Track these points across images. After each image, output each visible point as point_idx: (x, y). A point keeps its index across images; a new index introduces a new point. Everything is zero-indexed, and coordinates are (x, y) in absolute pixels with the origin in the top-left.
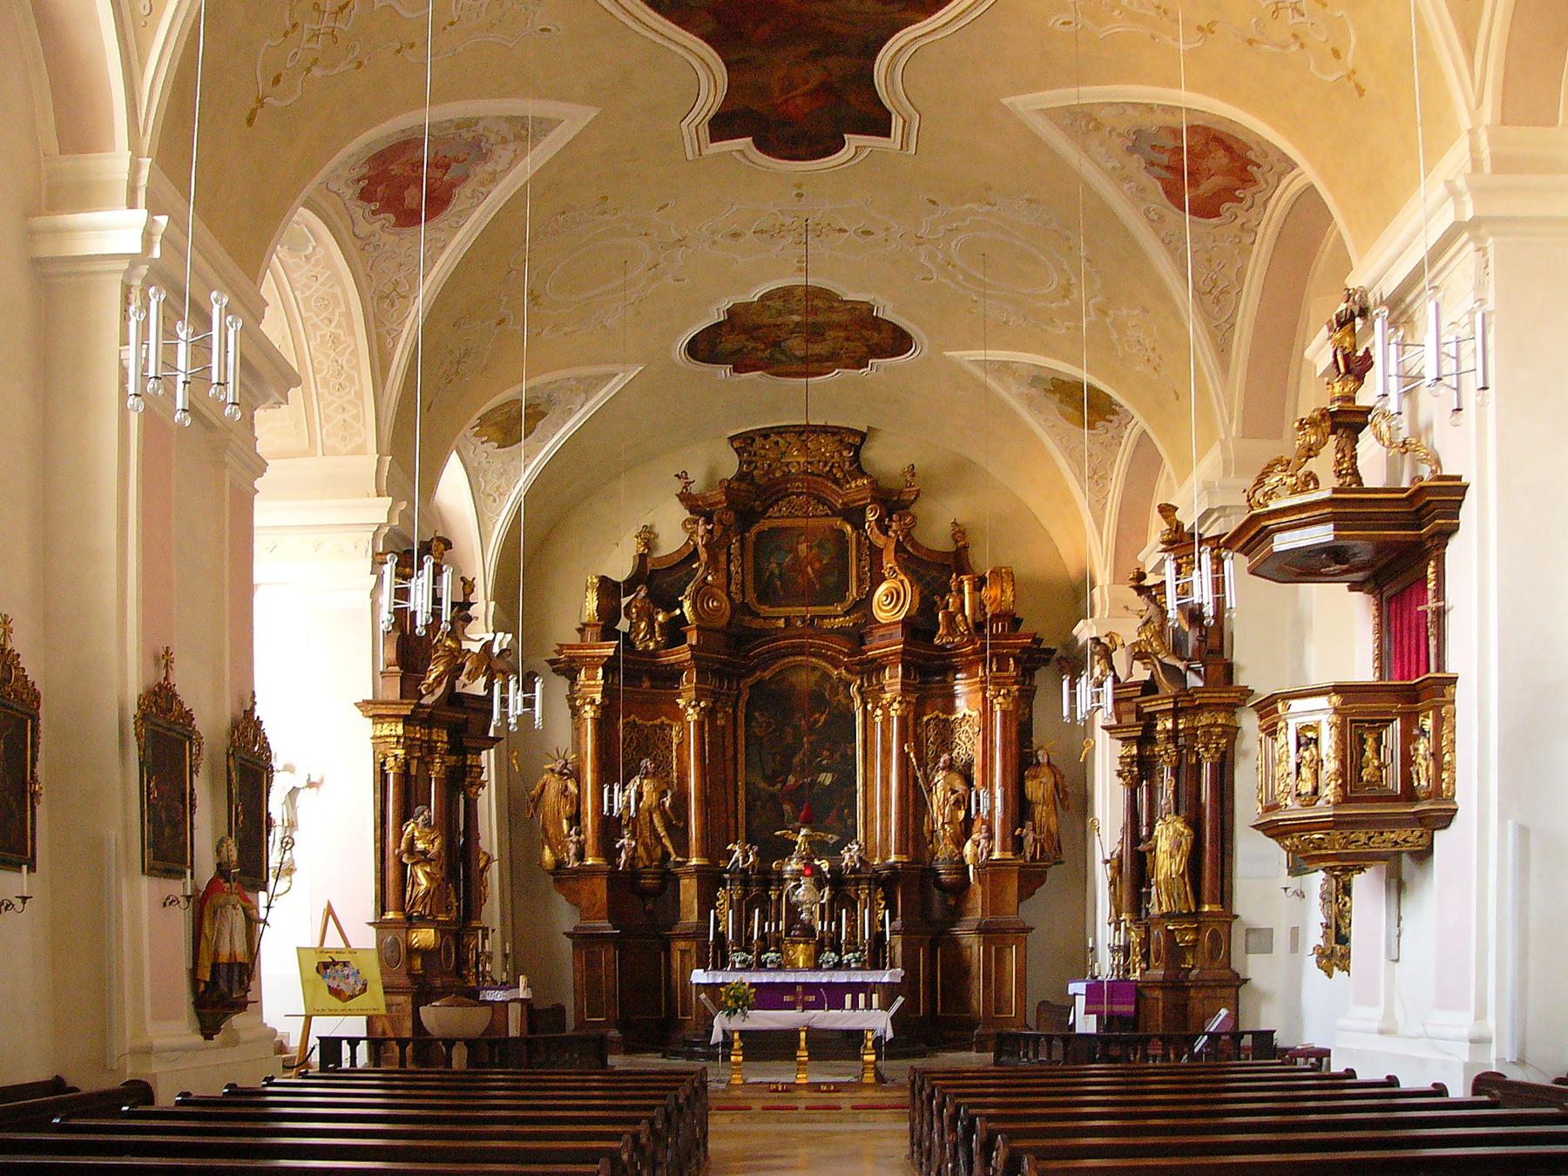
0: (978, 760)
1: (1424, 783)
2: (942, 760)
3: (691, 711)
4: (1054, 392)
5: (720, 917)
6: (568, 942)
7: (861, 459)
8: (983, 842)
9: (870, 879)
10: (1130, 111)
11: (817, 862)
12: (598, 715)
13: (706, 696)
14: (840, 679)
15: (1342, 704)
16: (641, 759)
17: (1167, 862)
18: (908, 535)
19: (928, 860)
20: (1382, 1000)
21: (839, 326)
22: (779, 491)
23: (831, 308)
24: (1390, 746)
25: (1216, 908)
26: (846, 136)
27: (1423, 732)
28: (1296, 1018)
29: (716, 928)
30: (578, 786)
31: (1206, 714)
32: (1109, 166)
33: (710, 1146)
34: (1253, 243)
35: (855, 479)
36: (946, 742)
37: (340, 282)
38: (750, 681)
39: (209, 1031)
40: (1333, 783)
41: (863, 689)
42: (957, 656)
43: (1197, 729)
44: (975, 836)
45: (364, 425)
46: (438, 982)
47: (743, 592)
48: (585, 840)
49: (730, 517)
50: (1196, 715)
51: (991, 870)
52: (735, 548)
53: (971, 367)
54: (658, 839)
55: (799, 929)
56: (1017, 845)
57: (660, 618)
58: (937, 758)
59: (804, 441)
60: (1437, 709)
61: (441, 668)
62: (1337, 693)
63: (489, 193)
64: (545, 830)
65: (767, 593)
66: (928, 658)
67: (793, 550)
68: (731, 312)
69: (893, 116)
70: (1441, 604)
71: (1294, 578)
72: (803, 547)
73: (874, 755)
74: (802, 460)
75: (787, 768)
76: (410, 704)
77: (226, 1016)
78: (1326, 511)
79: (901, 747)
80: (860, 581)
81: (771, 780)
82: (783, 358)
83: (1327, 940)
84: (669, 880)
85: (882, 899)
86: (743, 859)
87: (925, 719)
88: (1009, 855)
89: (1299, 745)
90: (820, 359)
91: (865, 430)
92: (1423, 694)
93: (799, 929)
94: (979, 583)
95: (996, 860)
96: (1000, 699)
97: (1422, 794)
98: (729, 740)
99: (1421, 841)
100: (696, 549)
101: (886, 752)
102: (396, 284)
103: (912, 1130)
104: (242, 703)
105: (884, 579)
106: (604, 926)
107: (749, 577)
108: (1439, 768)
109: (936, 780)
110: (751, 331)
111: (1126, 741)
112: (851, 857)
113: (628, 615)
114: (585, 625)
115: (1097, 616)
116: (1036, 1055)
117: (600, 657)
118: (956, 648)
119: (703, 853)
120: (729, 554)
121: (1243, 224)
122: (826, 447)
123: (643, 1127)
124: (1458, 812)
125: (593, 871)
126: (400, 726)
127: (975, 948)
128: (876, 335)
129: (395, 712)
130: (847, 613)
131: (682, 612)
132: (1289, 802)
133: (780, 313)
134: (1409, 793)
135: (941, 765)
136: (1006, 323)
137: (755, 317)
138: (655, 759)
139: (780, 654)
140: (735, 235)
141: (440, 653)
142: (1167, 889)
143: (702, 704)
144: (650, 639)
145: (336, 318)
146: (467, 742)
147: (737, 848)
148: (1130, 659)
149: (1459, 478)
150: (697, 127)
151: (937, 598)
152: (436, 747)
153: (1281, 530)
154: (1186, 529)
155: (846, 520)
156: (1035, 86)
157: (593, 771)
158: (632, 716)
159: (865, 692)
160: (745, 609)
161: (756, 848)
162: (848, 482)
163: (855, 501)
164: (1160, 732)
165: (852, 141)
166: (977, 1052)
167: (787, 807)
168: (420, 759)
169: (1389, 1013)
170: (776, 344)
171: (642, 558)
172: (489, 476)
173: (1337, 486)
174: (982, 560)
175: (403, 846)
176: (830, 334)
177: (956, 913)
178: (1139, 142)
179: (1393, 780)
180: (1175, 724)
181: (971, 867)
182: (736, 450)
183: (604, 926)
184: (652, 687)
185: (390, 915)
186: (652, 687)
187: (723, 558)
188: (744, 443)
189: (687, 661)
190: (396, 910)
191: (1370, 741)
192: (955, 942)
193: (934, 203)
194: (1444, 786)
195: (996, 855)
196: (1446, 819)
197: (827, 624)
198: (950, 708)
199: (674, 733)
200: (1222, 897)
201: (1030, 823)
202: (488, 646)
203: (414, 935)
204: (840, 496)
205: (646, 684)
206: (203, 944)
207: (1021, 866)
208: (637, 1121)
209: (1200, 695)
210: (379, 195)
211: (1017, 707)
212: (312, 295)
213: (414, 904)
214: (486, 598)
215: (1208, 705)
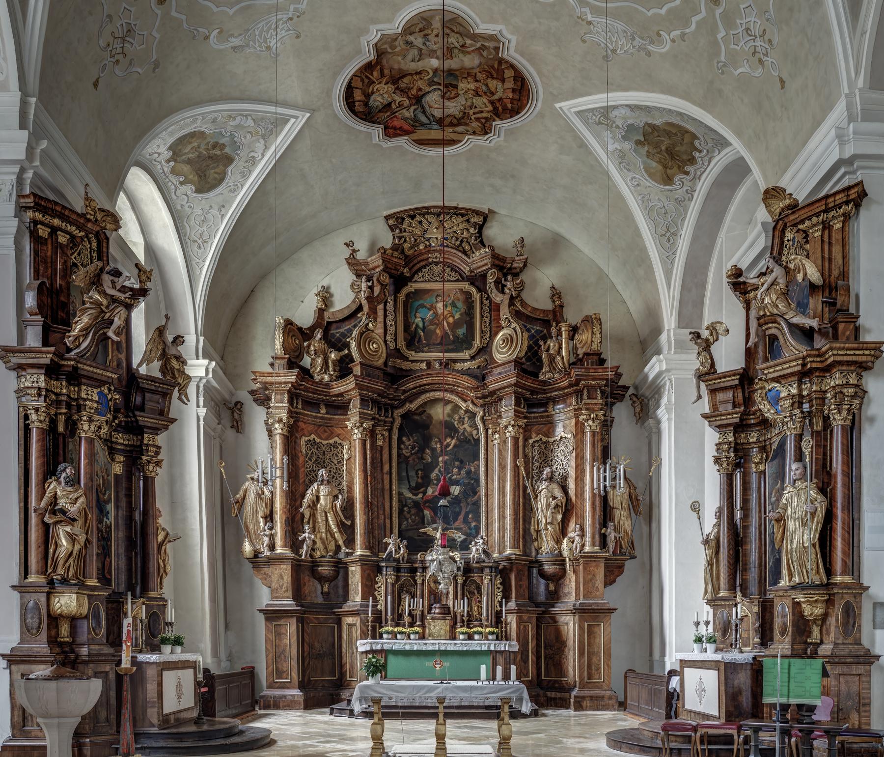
0: (572, 474)
2: (545, 472)
7: (483, 236)
8: (577, 538)
9: (491, 568)
12: (285, 432)
14: (467, 411)
16: (319, 470)
18: (519, 295)
19: (534, 554)
21: (468, 74)
25: (848, 579)
36: (546, 459)
38: (401, 411)
41: (485, 418)
47: (396, 340)
48: (276, 533)
49: (386, 279)
54: (333, 536)
55: (439, 608)
56: (603, 541)
57: (333, 356)
58: (541, 472)
59: (441, 221)
65: (412, 341)
66: (533, 392)
67: (432, 307)
72: (440, 305)
74: (440, 236)
75: (426, 482)
76: (49, 353)
80: (482, 332)
81: (414, 490)
82: (423, 119)
84: (341, 568)
85: (501, 584)
86: (396, 551)
87: (531, 441)
88: (597, 549)
93: (439, 608)
94: (574, 330)
95: (587, 553)
96: (590, 422)
101: (503, 467)
106: (288, 603)
107: (401, 328)
109: (540, 489)
112: (477, 550)
125: (280, 559)
126: (42, 377)
127: (571, 625)
128: (500, 85)
129: (35, 361)
130: (473, 358)
135: (544, 476)
138: (330, 471)
144: (325, 372)
151: (541, 343)
152: (147, 450)
155: (472, 284)
156: (575, 94)
158: (313, 436)
160: (397, 353)
161: (405, 542)
162: (473, 253)
166: (575, 710)
167: (427, 512)
170: (418, 100)
171: (321, 312)
172: (192, 223)
176: (463, 85)
177: (554, 596)
182: (390, 227)
183: (288, 603)
184: (327, 413)
186: (327, 413)
187: (380, 313)
188: (396, 221)
190: (38, 573)
192: (554, 620)
195: (587, 549)
197: (458, 366)
199: (344, 451)
201: (612, 524)
203: (57, 600)
207: (607, 559)
209: (835, 352)
214: (196, 333)
215: (840, 363)
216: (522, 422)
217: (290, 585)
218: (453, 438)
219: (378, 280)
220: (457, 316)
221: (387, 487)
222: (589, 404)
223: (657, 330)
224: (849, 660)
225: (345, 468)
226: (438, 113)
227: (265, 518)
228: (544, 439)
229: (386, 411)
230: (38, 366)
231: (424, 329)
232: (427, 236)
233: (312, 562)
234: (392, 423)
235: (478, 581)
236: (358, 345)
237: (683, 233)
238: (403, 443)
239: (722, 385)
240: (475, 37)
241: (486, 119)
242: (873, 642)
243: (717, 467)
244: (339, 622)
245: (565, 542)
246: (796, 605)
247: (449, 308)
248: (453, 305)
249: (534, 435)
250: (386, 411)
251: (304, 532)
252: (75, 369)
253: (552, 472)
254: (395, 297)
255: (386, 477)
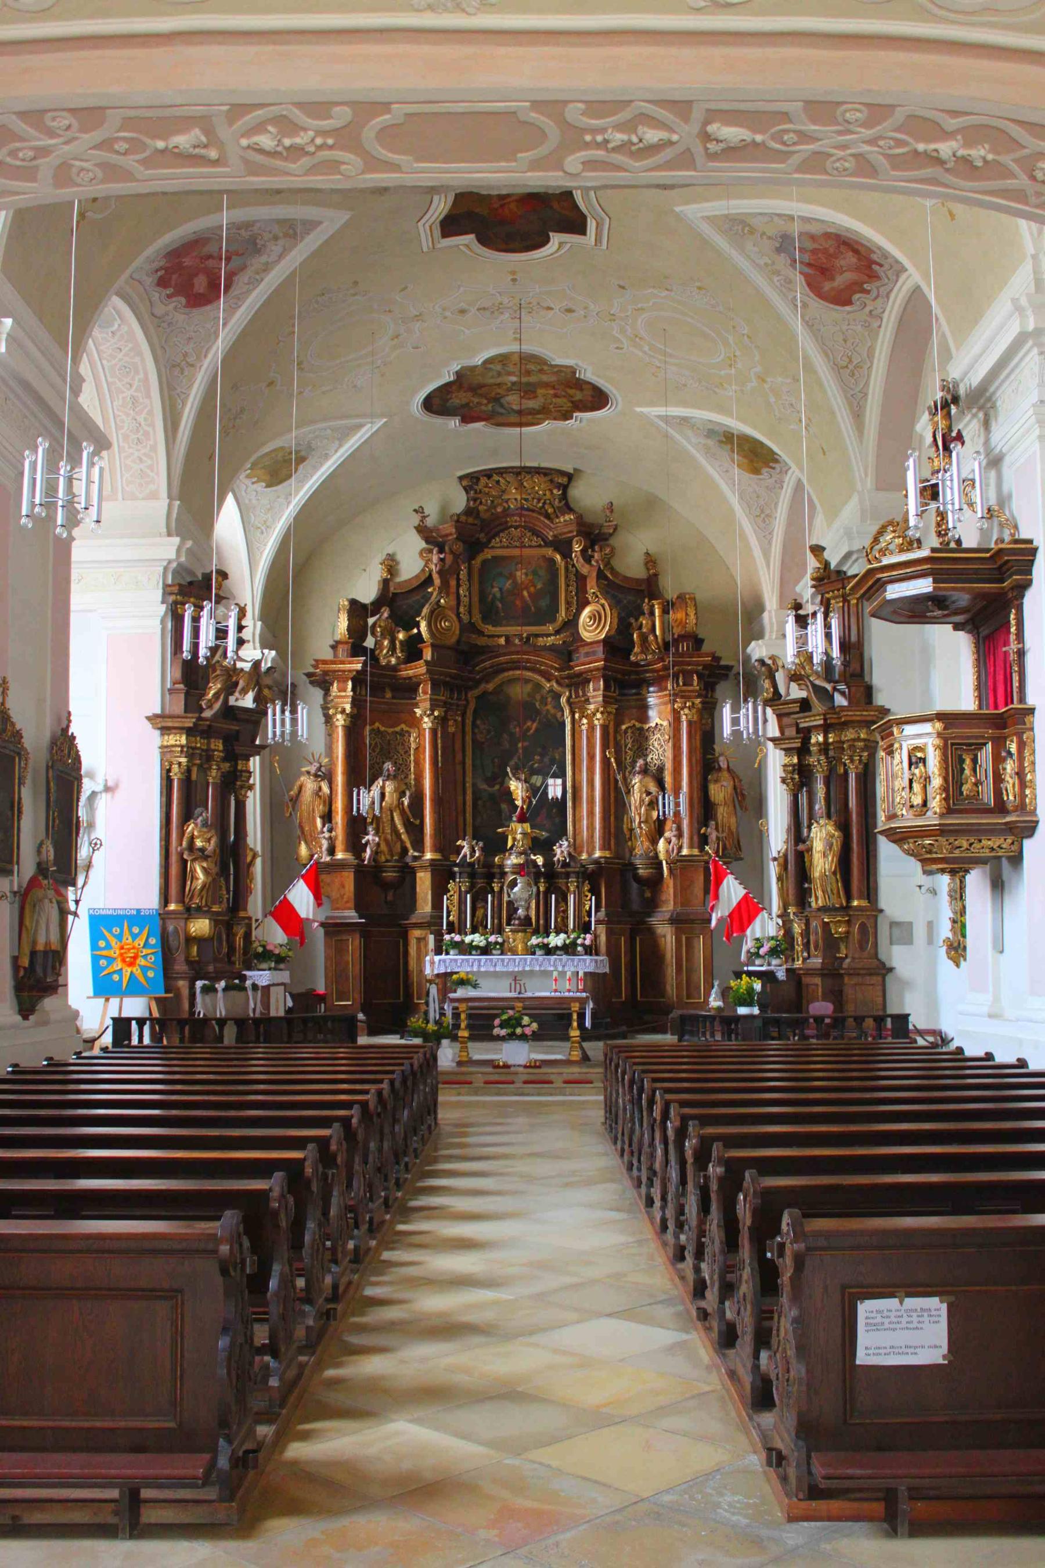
0: (669, 766)
1: (1011, 798)
3: (426, 719)
4: (726, 443)
5: (451, 907)
6: (321, 931)
8: (674, 839)
9: (577, 873)
10: (776, 218)
11: (533, 857)
13: (438, 706)
14: (551, 691)
15: (945, 729)
16: (384, 763)
17: (821, 861)
18: (607, 564)
19: (627, 855)
20: (991, 989)
21: (547, 385)
22: (501, 524)
23: (541, 371)
24: (984, 766)
25: (864, 903)
26: (551, 234)
27: (1010, 754)
28: (933, 1004)
29: (448, 916)
30: (331, 788)
31: (851, 730)
32: (762, 262)
33: (440, 1116)
34: (880, 327)
35: (563, 515)
36: (641, 748)
37: (140, 354)
38: (476, 692)
39: (26, 1010)
40: (938, 797)
42: (647, 671)
43: (844, 743)
44: (667, 834)
45: (157, 474)
46: (211, 968)
48: (336, 837)
49: (459, 547)
50: (842, 730)
51: (680, 865)
52: (463, 574)
53: (656, 420)
54: (398, 835)
57: (401, 636)
58: (634, 762)
60: (1020, 735)
61: (219, 686)
62: (939, 720)
63: (262, 280)
64: (301, 827)
65: (490, 614)
66: (624, 673)
67: (512, 576)
68: (459, 374)
69: (589, 220)
70: (1020, 646)
71: (907, 620)
72: (518, 574)
73: (581, 761)
74: (519, 497)
77: (41, 998)
78: (925, 567)
79: (603, 752)
80: (568, 603)
82: (502, 411)
83: (955, 934)
84: (408, 873)
85: (589, 891)
87: (624, 727)
88: (696, 852)
89: (910, 764)
90: (533, 412)
91: (572, 471)
92: (1009, 721)
96: (686, 711)
97: (1010, 807)
98: (458, 745)
99: (1014, 848)
100: (430, 575)
101: (591, 757)
102: (185, 355)
103: (606, 1101)
104: (59, 720)
105: (588, 603)
106: (351, 915)
107: (476, 599)
108: (1023, 784)
110: (475, 389)
111: (788, 751)
112: (562, 852)
113: (373, 634)
114: (338, 643)
115: (767, 637)
116: (713, 1035)
117: (350, 671)
118: (648, 665)
119: (436, 849)
120: (458, 580)
121: (871, 312)
122: (539, 486)
123: (385, 1086)
124: (1040, 824)
125: (341, 865)
126: (184, 737)
128: (578, 392)
130: (557, 632)
131: (419, 632)
132: (904, 812)
133: (499, 374)
134: (1001, 807)
136: (685, 385)
137: (480, 378)
139: (500, 670)
140: (462, 312)
141: (218, 672)
142: (822, 886)
143: (436, 713)
144: (392, 655)
145: (136, 384)
146: (239, 749)
147: (465, 843)
148: (787, 680)
149: (1030, 542)
150: (431, 227)
151: (632, 620)
153: (892, 581)
154: (832, 567)
155: (557, 549)
157: (343, 773)
158: (377, 724)
159: (574, 703)
161: (481, 844)
162: (557, 517)
163: (565, 533)
164: (814, 745)
165: (556, 238)
168: (200, 766)
169: (996, 999)
170: (497, 400)
171: (386, 583)
173: (938, 546)
174: (670, 588)
175: (185, 844)
176: (540, 391)
177: (652, 905)
178: (784, 244)
179: (988, 796)
180: (826, 737)
181: (664, 863)
183: (351, 915)
184: (393, 697)
185: (172, 907)
186: (393, 697)
187: (453, 583)
188: (471, 482)
189: (423, 675)
191: (968, 761)
192: (651, 931)
193: (623, 288)
194: (1027, 800)
195: (685, 852)
196: (1030, 829)
197: (541, 641)
198: (644, 718)
199: (412, 739)
200: (868, 895)
202: (257, 664)
204: (551, 529)
205: (389, 695)
206: (24, 935)
208: (381, 1081)
210: (173, 283)
211: (701, 718)
212: (116, 365)
213: (192, 897)
214: (254, 618)
215: (852, 722)
216: (612, 709)
217: (352, 895)
218: (534, 721)
219: (450, 549)
220: (539, 586)
221: (459, 778)
222: (684, 691)
223: (760, 608)
224: (862, 972)
225: (412, 758)
226: (516, 407)
227: (322, 817)
228: (638, 725)
229: (459, 693)
230: (182, 728)
231: (502, 600)
232: (505, 497)
233: (375, 867)
234: (466, 706)
235: (564, 888)
236: (429, 625)
237: (778, 515)
238: (478, 727)
239: (787, 711)
240: (551, 366)
241: (567, 411)
242: (890, 958)
243: (785, 786)
244: (405, 936)
245: (662, 841)
246: (826, 925)
247: (530, 577)
248: (535, 573)
249: (627, 720)
250: (459, 693)
251: (367, 834)
252: (210, 726)
253: (646, 764)
254: (470, 565)
255: (459, 768)
